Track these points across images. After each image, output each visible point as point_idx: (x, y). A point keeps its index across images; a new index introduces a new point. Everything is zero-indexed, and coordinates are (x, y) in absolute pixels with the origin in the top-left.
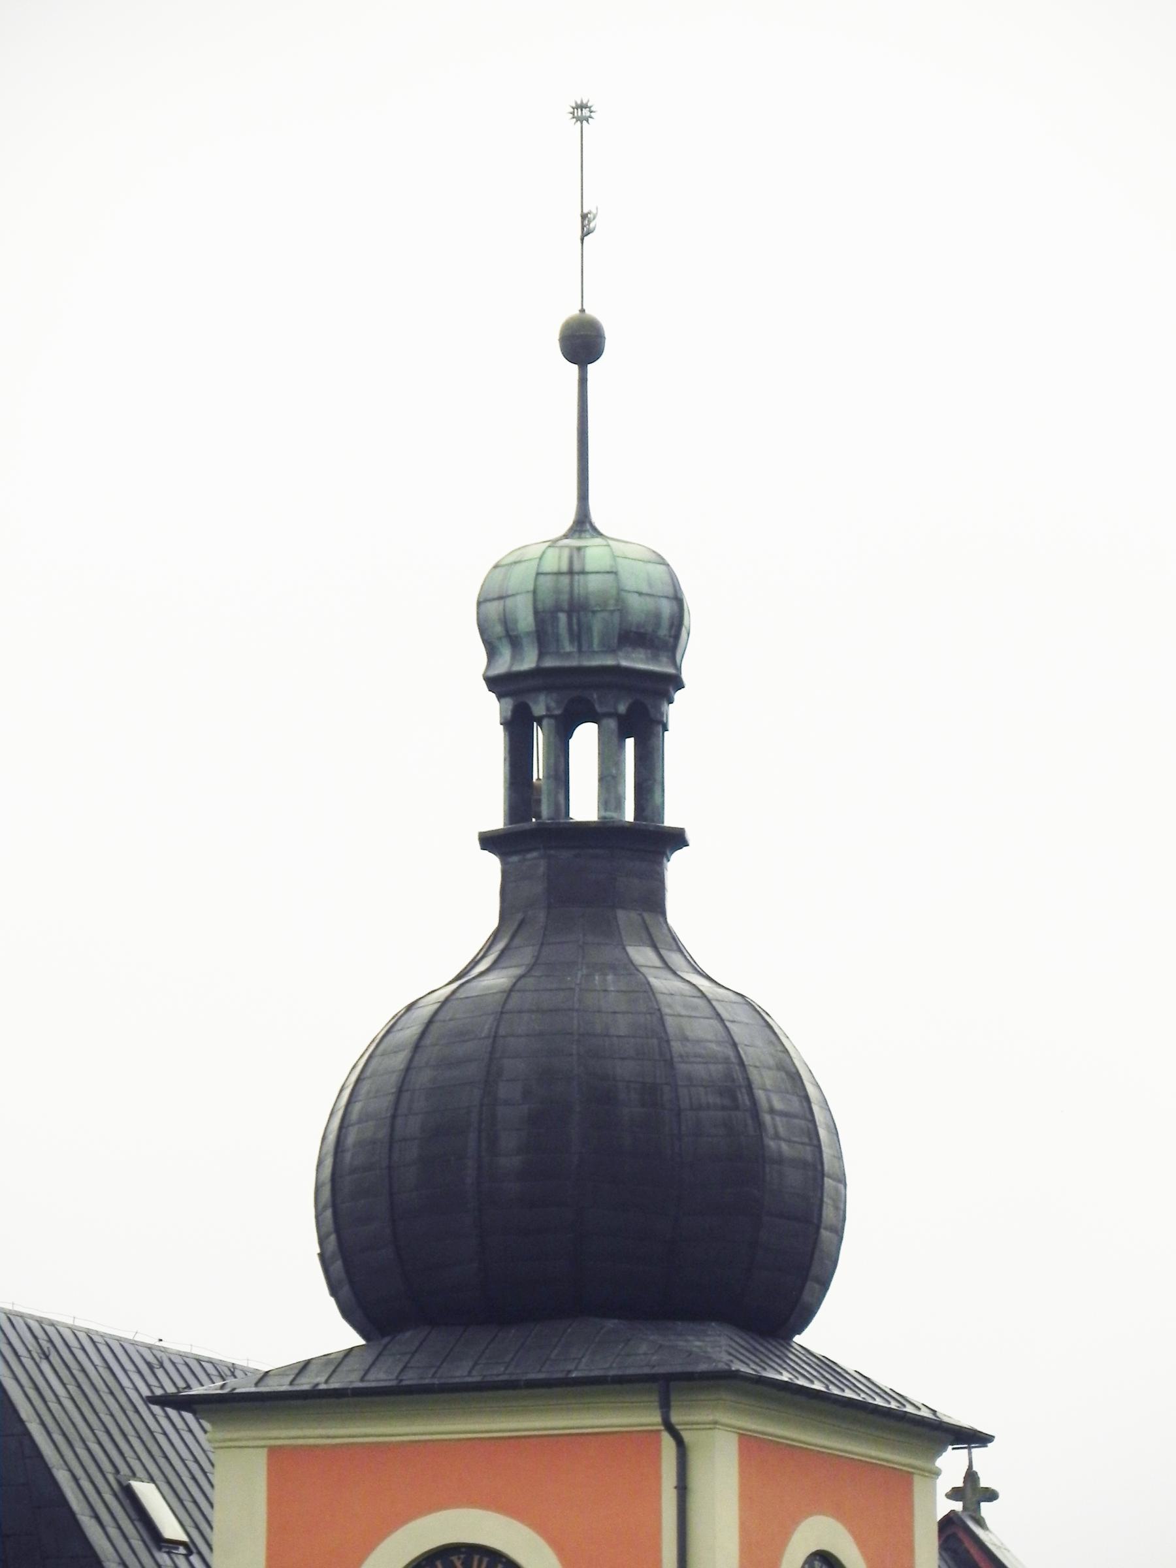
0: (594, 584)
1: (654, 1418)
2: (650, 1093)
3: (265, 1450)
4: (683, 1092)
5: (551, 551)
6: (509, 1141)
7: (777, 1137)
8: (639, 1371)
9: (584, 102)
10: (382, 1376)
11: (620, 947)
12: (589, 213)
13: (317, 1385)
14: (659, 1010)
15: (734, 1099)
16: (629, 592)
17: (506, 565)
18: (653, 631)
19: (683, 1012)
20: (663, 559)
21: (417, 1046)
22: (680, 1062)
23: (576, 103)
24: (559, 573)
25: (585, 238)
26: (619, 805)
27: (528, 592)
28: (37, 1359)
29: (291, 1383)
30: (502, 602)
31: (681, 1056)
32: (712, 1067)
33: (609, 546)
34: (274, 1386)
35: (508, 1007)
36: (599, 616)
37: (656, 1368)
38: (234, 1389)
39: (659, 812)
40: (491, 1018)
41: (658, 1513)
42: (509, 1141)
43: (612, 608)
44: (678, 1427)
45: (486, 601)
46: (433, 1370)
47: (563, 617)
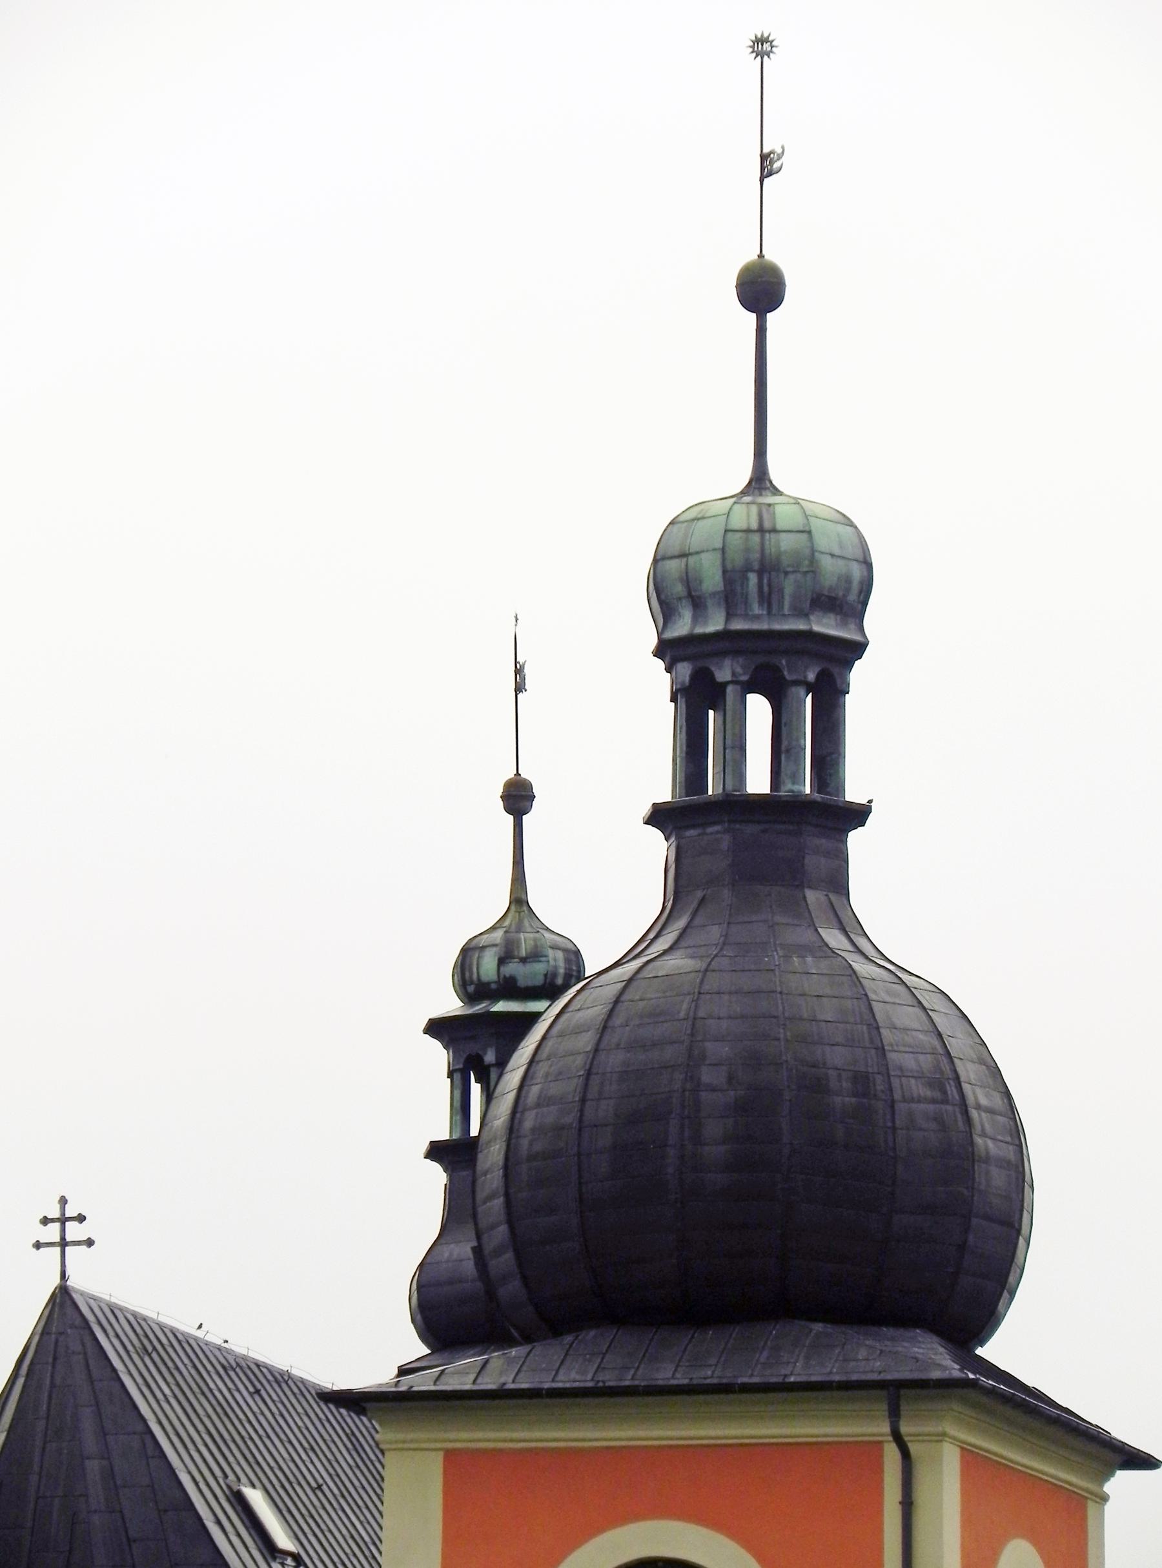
0: (786, 543)
1: (884, 1428)
2: (862, 1082)
3: (441, 1454)
4: (895, 1082)
5: (737, 507)
6: (713, 1129)
7: (984, 1134)
8: (864, 1377)
9: (766, 35)
10: (573, 1375)
11: (812, 929)
12: (772, 152)
13: (504, 1384)
14: (866, 995)
15: (945, 1092)
16: (823, 553)
17: (687, 521)
18: (844, 595)
19: (888, 999)
20: (849, 519)
21: (605, 1027)
22: (890, 1051)
23: (762, 35)
24: (748, 531)
25: (766, 181)
26: (797, 778)
27: (714, 550)
28: (142, 1355)
29: (474, 1382)
30: (684, 560)
31: (892, 1045)
32: (921, 1057)
33: (799, 503)
34: (454, 1384)
35: (706, 987)
36: (792, 577)
37: (882, 1375)
38: (412, 1387)
39: (840, 789)
40: (688, 999)
41: (879, 1530)
42: (713, 1129)
43: (805, 569)
44: (906, 1439)
45: (664, 558)
46: (632, 1372)
47: (753, 578)
